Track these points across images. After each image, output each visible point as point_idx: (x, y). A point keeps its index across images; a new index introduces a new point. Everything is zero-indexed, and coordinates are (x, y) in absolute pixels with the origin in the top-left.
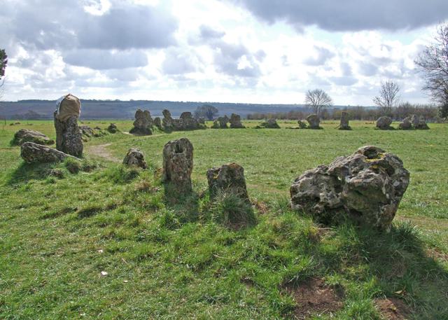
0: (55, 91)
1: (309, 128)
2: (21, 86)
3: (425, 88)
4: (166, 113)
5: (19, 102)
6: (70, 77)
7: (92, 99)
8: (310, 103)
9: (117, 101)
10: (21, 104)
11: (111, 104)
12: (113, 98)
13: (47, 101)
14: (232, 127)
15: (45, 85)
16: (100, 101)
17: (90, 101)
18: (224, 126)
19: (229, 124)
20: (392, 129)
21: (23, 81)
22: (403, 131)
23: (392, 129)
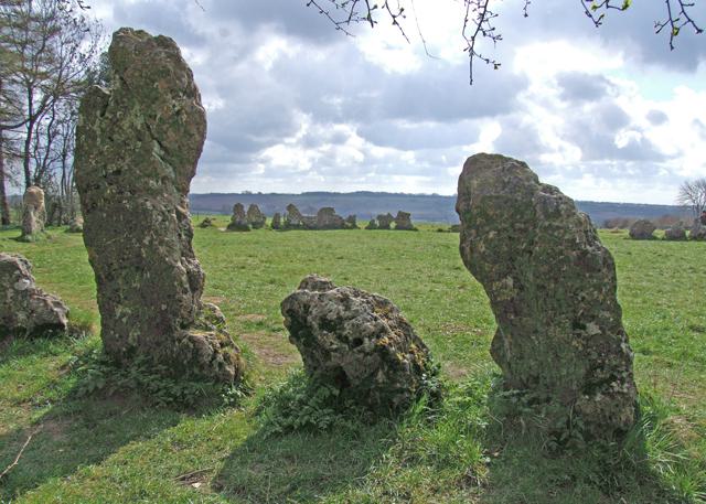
0: (348, 180)
1: (379, 228)
2: (305, 173)
3: (686, 183)
4: (290, 207)
5: (303, 194)
6: (369, 162)
7: (255, 192)
8: (688, 202)
9: (434, 196)
10: (318, 198)
11: (426, 199)
12: (429, 191)
13: (338, 194)
14: (397, 228)
15: (340, 172)
16: (410, 195)
17: (396, 194)
18: (387, 227)
19: (393, 225)
20: (655, 238)
21: (308, 166)
22: (671, 243)
23: (655, 238)
